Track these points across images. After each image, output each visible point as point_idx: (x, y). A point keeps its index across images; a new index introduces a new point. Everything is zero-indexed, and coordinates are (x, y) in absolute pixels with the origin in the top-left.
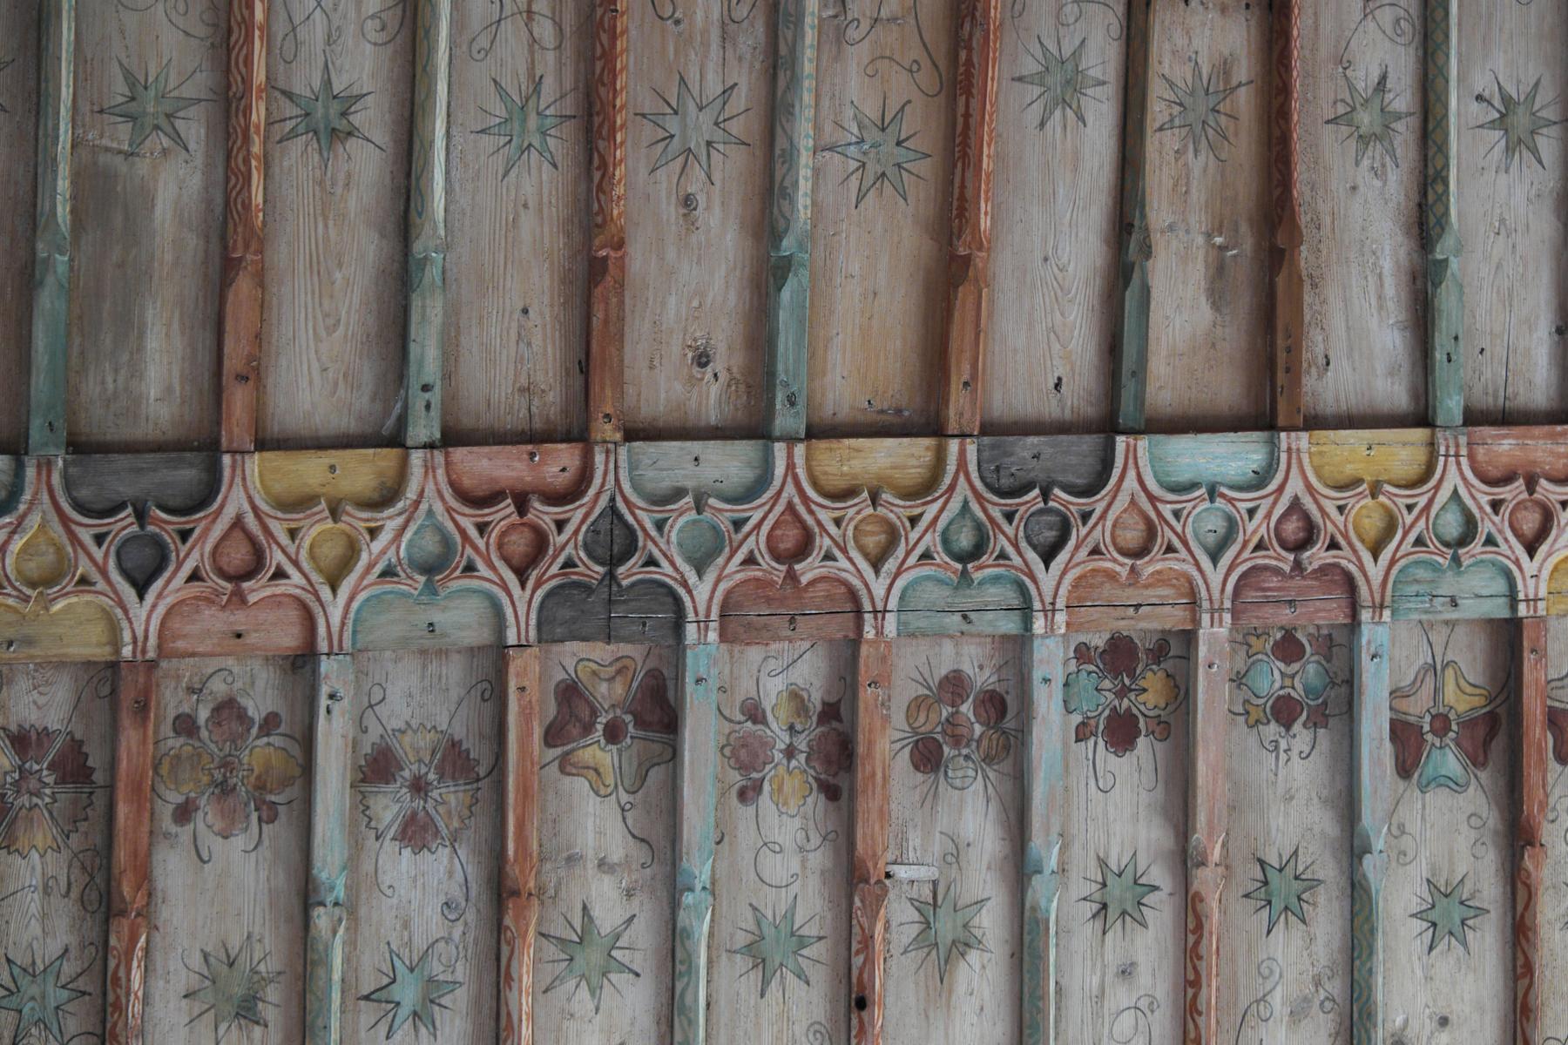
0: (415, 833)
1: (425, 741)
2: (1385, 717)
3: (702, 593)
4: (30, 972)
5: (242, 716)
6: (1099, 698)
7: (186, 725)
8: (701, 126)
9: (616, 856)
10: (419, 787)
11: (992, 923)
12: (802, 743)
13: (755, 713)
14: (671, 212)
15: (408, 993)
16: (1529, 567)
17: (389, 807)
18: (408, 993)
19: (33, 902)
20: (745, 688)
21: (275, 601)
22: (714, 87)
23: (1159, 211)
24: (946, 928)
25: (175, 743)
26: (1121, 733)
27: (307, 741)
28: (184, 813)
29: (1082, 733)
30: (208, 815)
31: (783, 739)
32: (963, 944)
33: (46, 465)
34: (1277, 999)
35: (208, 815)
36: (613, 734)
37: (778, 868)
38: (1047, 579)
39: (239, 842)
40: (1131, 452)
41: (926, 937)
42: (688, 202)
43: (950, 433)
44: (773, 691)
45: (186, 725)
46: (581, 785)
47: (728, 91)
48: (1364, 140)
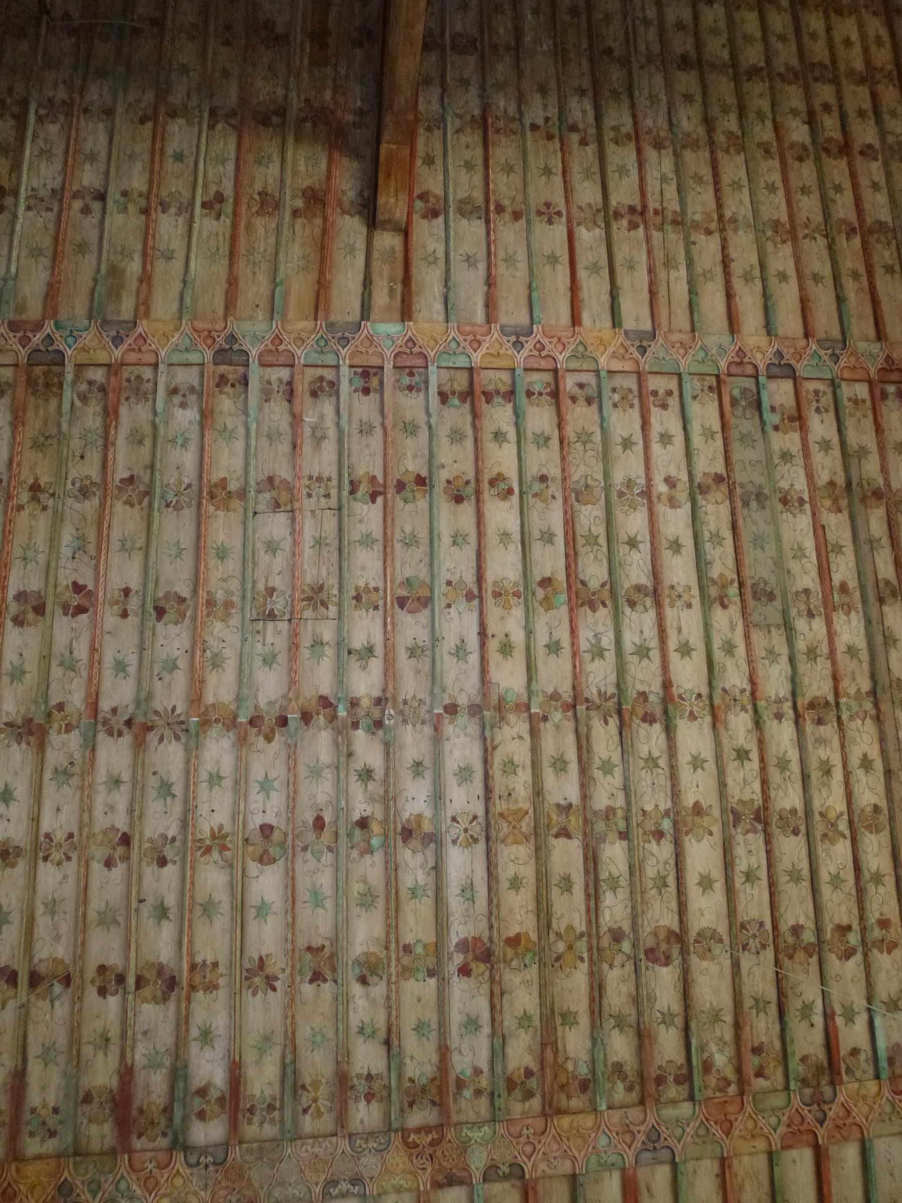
0: (183, 405)
1: (186, 386)
2: (436, 390)
3: (254, 352)
4: (90, 431)
5: (142, 379)
6: (359, 383)
7: (128, 380)
8: (258, 257)
9: (233, 412)
10: (184, 396)
11: (332, 432)
12: (281, 390)
13: (269, 383)
14: (250, 274)
15: (180, 441)
16: (475, 355)
17: (177, 399)
18: (180, 441)
19: (91, 417)
20: (267, 377)
21: (149, 351)
22: (262, 249)
23: (375, 277)
24: (318, 434)
25: (125, 384)
26: (366, 391)
27: (156, 384)
28: (127, 399)
29: (355, 391)
30: (133, 400)
31: (276, 389)
32: (323, 437)
33: (96, 322)
34: (408, 454)
35: (133, 400)
36: (233, 386)
37: (276, 417)
38: (343, 352)
39: (140, 406)
40: (365, 325)
41: (313, 435)
42: (254, 273)
43: (758, 797)
44: (274, 378)
45: (128, 380)
46: (224, 397)
47: (265, 250)
48: (430, 263)
